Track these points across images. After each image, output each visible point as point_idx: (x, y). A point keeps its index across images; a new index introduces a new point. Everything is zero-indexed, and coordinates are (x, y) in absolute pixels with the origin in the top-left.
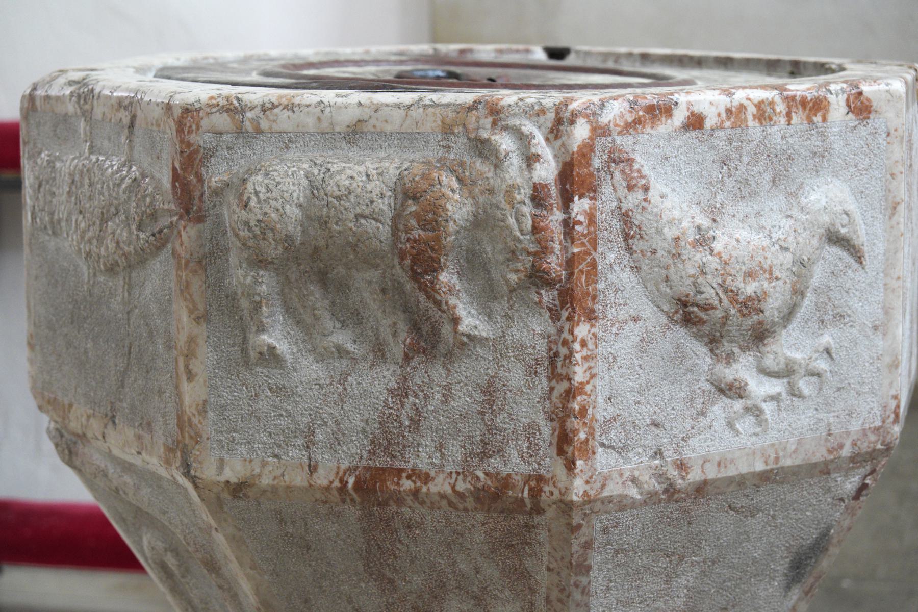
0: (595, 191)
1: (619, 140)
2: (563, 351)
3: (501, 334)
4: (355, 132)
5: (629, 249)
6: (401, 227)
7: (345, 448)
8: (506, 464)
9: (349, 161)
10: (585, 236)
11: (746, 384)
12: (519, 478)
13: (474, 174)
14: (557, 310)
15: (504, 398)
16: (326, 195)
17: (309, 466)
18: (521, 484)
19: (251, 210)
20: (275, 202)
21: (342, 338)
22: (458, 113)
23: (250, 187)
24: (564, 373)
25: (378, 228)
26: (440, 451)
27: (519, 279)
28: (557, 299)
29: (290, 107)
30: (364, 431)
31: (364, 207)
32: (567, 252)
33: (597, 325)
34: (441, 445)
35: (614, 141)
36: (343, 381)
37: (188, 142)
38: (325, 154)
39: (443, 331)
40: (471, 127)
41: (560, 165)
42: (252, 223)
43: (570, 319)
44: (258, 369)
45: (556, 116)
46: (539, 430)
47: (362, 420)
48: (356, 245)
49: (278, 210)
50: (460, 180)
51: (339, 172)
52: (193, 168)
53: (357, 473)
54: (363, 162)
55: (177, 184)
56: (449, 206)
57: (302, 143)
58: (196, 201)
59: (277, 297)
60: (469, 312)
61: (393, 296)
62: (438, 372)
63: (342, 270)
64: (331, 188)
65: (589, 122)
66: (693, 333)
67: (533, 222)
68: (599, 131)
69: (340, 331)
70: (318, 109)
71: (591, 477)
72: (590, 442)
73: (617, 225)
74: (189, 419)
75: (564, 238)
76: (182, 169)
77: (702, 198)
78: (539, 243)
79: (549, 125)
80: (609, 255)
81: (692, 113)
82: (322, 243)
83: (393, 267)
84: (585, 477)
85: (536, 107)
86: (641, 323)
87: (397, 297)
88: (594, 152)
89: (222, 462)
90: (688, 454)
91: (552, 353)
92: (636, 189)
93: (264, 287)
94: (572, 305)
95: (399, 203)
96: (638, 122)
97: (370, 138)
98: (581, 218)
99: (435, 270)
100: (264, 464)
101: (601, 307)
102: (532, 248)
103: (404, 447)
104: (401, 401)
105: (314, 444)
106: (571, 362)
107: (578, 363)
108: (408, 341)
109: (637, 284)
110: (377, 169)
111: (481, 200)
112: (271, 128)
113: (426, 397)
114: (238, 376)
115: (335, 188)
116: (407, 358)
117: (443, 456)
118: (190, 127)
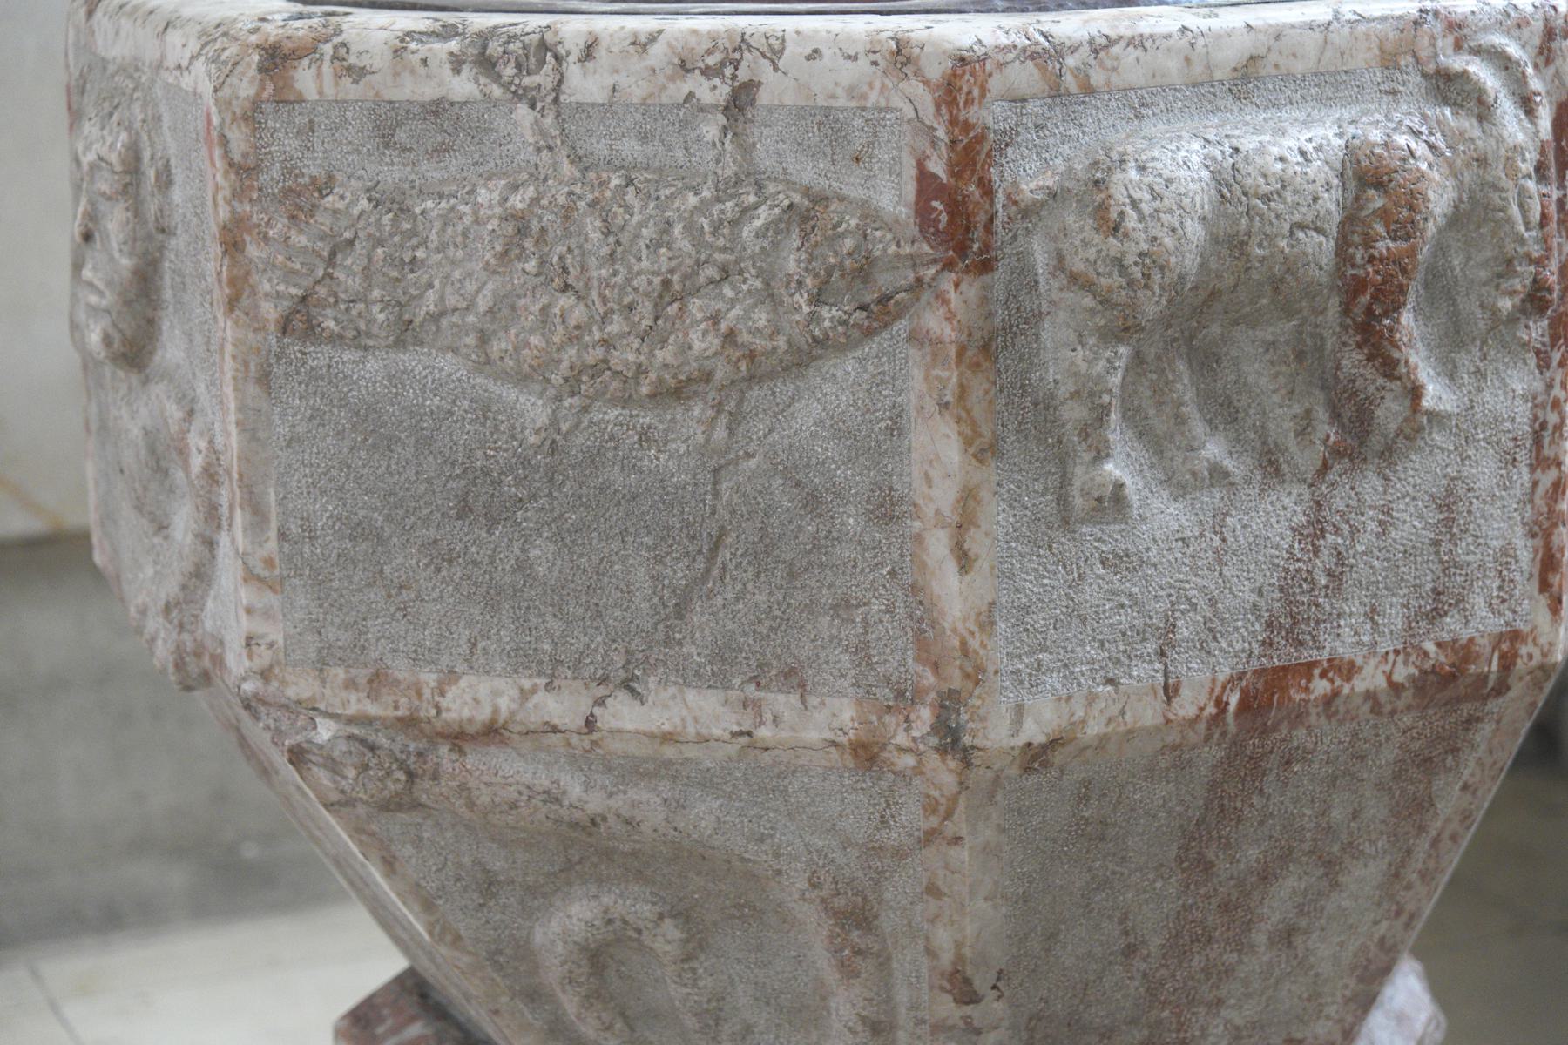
2: (1553, 418)
4: (1246, 78)
6: (1356, 238)
7: (1224, 645)
11: (876, 917)
17: (1166, 687)
18: (1488, 649)
19: (1126, 235)
21: (1214, 450)
23: (1119, 194)
24: (1552, 455)
25: (1320, 245)
26: (1372, 619)
29: (1137, 42)
31: (1304, 210)
34: (1373, 610)
37: (966, 122)
39: (1378, 412)
40: (1423, 54)
42: (1131, 259)
44: (1085, 529)
47: (1252, 591)
49: (1173, 230)
51: (1261, 150)
52: (973, 171)
53: (1244, 683)
55: (936, 204)
56: (1431, 194)
57: (1162, 106)
58: (979, 233)
62: (1370, 485)
74: (964, 643)
79: (1537, 41)
89: (1019, 710)
91: (1537, 426)
95: (1351, 196)
100: (1091, 699)
112: (1108, 83)
114: (1050, 547)
115: (1261, 180)
116: (1325, 467)
118: (969, 92)
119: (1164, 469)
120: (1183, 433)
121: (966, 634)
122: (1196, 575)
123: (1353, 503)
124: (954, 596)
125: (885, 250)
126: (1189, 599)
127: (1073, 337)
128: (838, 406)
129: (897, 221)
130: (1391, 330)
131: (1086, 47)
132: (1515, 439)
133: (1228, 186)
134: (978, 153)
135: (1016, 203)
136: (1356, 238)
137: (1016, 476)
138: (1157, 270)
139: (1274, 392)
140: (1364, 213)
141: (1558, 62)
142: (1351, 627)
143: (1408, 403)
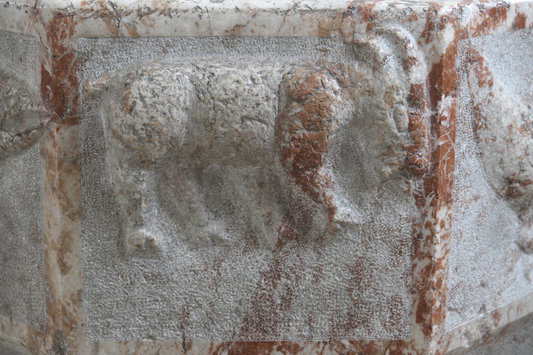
0: (456, 89)
1: (473, 40)
2: (426, 232)
3: (370, 220)
4: (233, 37)
5: (477, 139)
6: (286, 127)
7: (219, 327)
8: (369, 333)
9: (230, 65)
10: (447, 129)
12: (381, 344)
13: (353, 76)
14: (422, 197)
15: (371, 276)
16: (213, 98)
17: (184, 344)
18: (383, 348)
19: (136, 114)
20: (162, 107)
21: (216, 227)
22: (334, 18)
23: (134, 92)
25: (263, 129)
26: (309, 324)
27: (393, 171)
28: (423, 187)
30: (237, 310)
31: (250, 110)
32: (433, 145)
33: (452, 207)
34: (310, 320)
35: (470, 41)
36: (217, 266)
38: (204, 58)
39: (315, 218)
40: (346, 31)
41: (431, 66)
42: (138, 127)
43: (433, 204)
44: (134, 260)
45: (428, 21)
46: (401, 302)
47: (235, 301)
48: (240, 145)
49: (165, 114)
50: (340, 82)
51: (226, 76)
52: (66, 72)
53: (230, 348)
54: (245, 67)
55: (48, 87)
56: (333, 107)
57: (180, 47)
58: (70, 104)
59: (154, 193)
60: (343, 202)
61: (270, 189)
62: (309, 256)
63: (216, 166)
64: (218, 92)
65: (454, 26)
66: (511, 204)
67: (410, 120)
68: (461, 34)
69: (214, 222)
70: (196, 15)
71: (441, 338)
72: (442, 309)
73: (469, 117)
74: (64, 308)
75: (432, 133)
76: (54, 73)
77: (522, 88)
78: (414, 138)
79: (421, 30)
80: (463, 145)
81: (519, 15)
82: (206, 143)
83: (273, 163)
84: (438, 339)
85: (408, 13)
86: (479, 201)
87: (273, 190)
88: (457, 53)
90: (502, 305)
91: (415, 235)
92: (484, 85)
93: (145, 185)
94: (436, 191)
95: (283, 105)
96: (485, 24)
97: (248, 42)
98: (446, 114)
99: (316, 166)
100: (139, 345)
101: (455, 191)
102: (407, 143)
103: (276, 322)
104: (273, 282)
105: (188, 324)
106: (432, 242)
107: (438, 242)
108: (283, 229)
109: (479, 168)
110: (261, 72)
111: (361, 100)
112: (147, 33)
113: (298, 278)
114: (114, 267)
115: (222, 92)
116: (280, 244)
117: (311, 328)
118: (64, 31)
119: (186, 234)
120: (194, 217)
121: (65, 304)
122: (202, 290)
123: (298, 263)
124: (63, 286)
125: (26, 107)
126: (197, 302)
127: (117, 163)
128: (17, 181)
129: (34, 93)
130: (312, 177)
131: (135, 13)
132: (402, 241)
133: (203, 93)
134: (69, 63)
135: (86, 91)
136: (286, 127)
137: (93, 229)
138: (156, 134)
139: (252, 201)
140: (290, 114)
141: (434, 42)
142: (297, 327)
143: (327, 215)
